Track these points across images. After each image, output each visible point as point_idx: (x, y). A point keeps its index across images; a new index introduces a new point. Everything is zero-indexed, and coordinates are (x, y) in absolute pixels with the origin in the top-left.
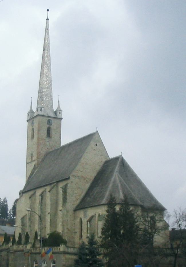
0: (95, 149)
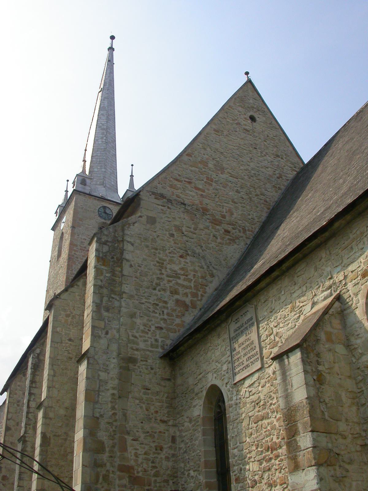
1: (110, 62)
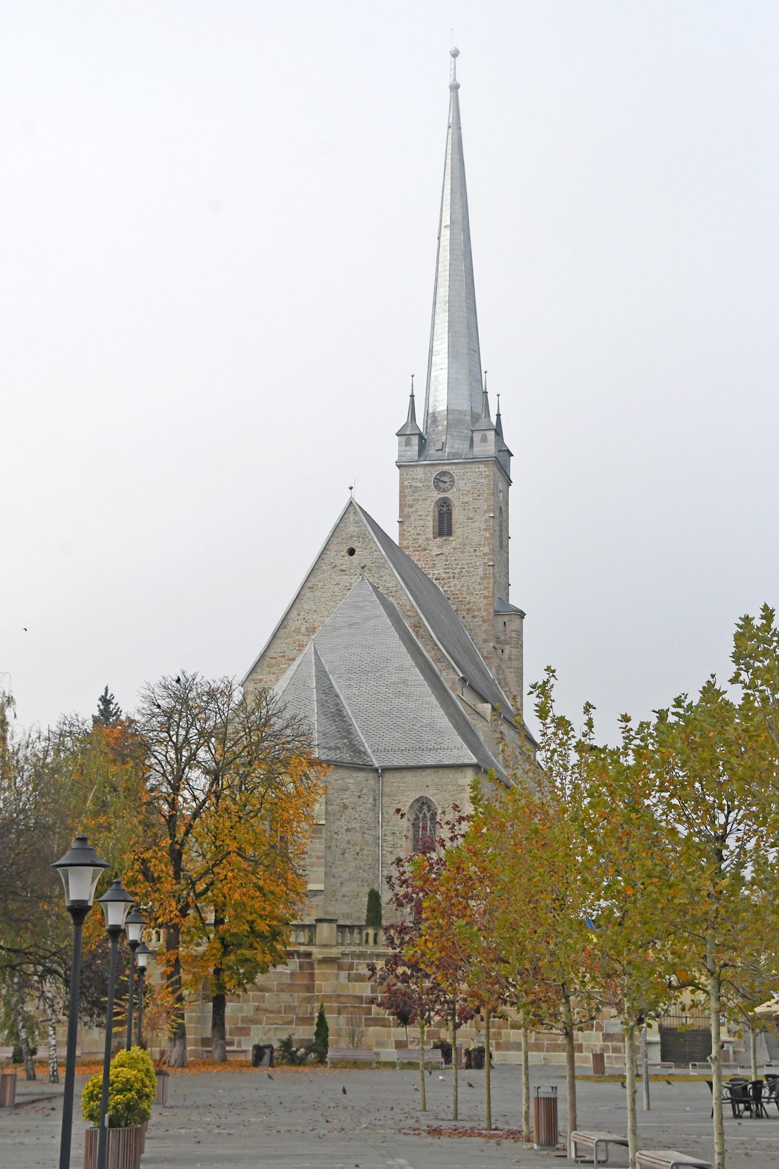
0: (344, 567)
1: (456, 127)
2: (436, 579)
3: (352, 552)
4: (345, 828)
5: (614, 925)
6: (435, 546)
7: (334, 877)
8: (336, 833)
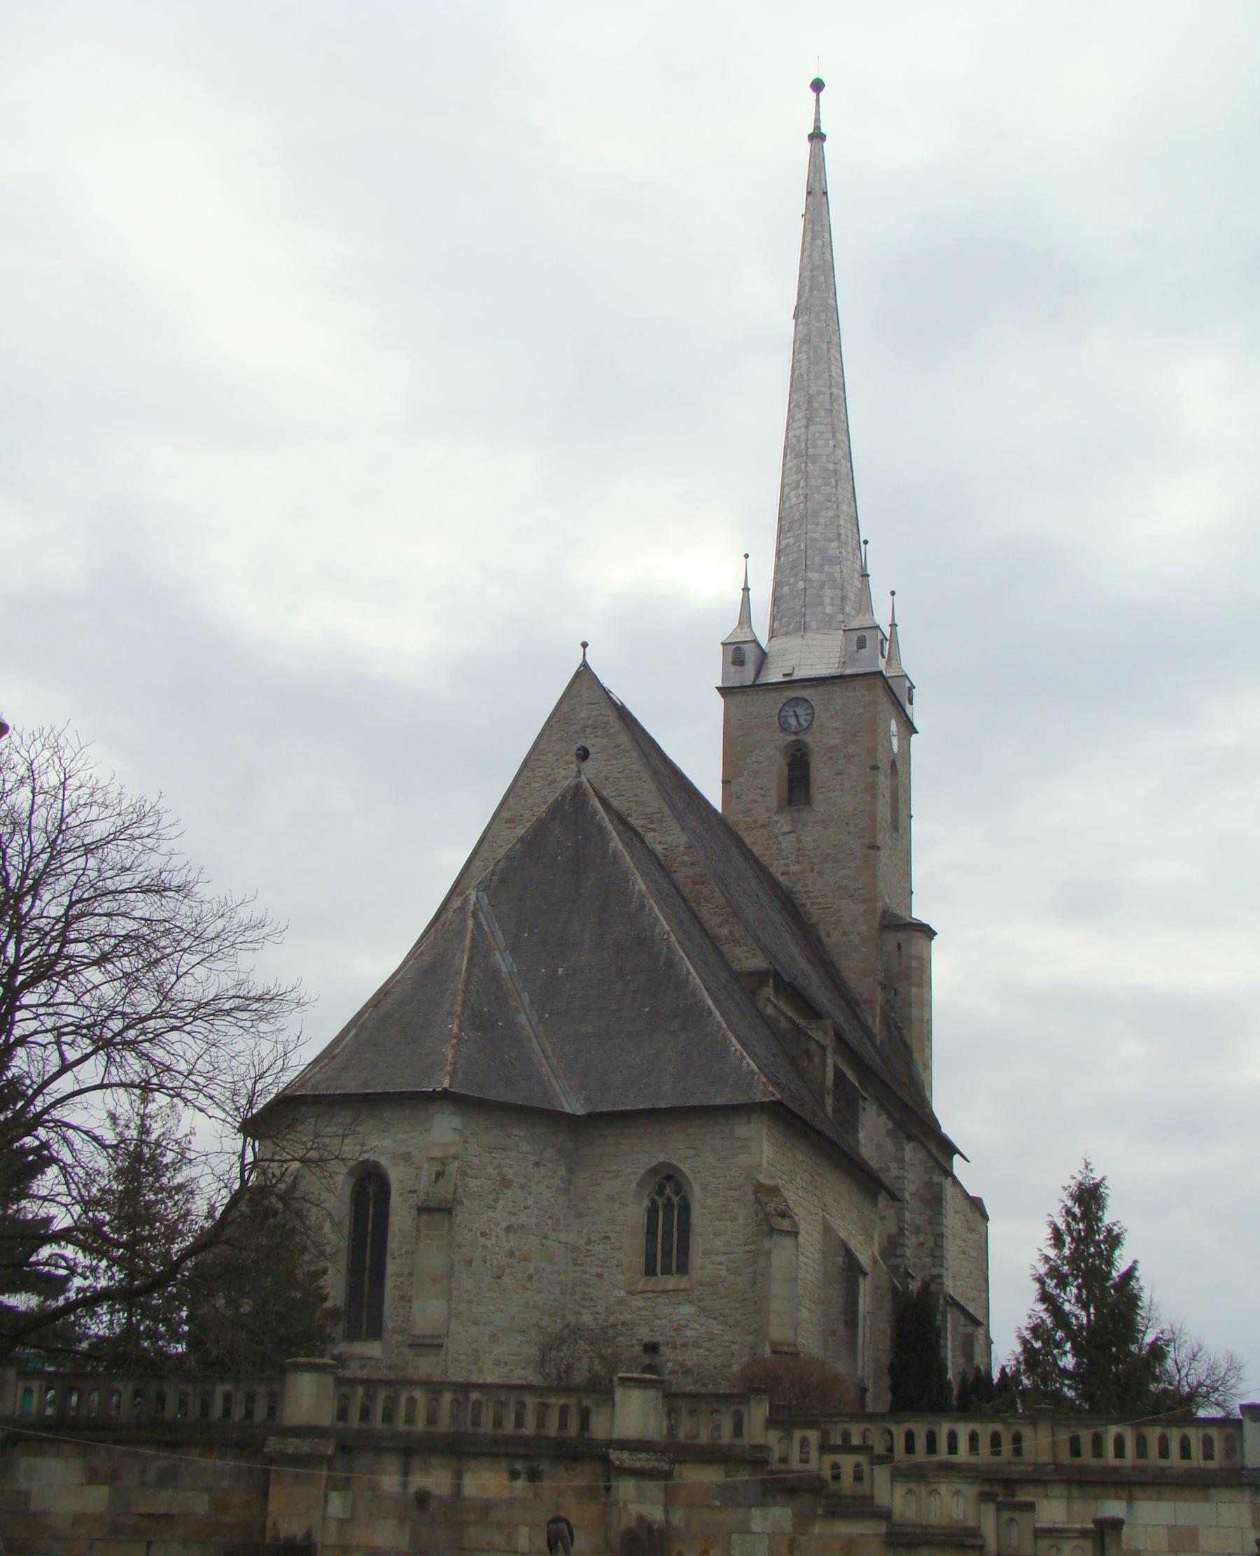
1: (817, 194)
2: (783, 874)
3: (584, 755)
4: (504, 1225)
5: (499, 1174)
6: (783, 823)
7: (476, 1322)
8: (483, 1234)
